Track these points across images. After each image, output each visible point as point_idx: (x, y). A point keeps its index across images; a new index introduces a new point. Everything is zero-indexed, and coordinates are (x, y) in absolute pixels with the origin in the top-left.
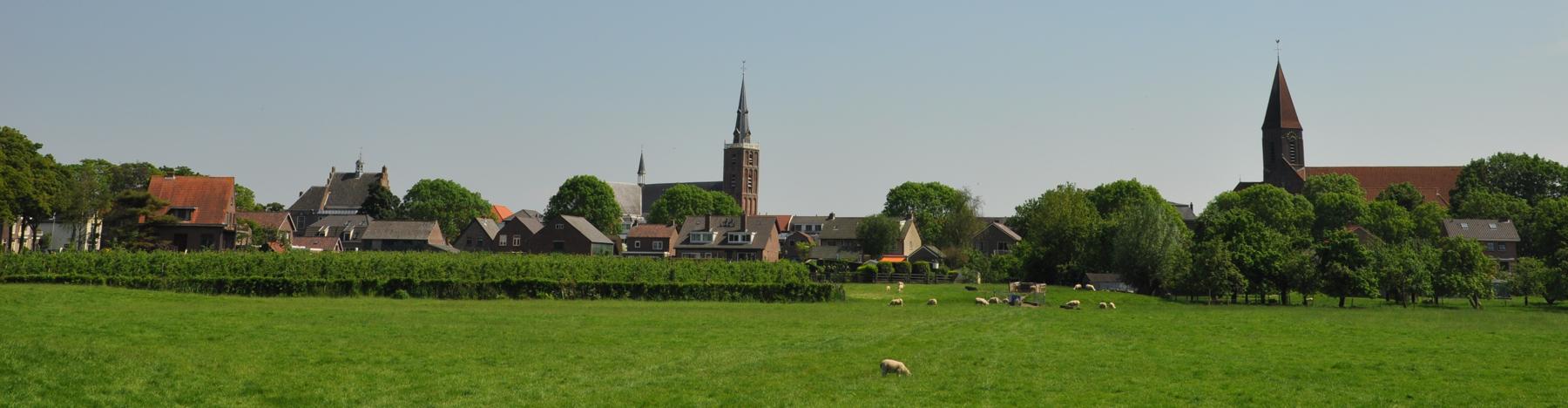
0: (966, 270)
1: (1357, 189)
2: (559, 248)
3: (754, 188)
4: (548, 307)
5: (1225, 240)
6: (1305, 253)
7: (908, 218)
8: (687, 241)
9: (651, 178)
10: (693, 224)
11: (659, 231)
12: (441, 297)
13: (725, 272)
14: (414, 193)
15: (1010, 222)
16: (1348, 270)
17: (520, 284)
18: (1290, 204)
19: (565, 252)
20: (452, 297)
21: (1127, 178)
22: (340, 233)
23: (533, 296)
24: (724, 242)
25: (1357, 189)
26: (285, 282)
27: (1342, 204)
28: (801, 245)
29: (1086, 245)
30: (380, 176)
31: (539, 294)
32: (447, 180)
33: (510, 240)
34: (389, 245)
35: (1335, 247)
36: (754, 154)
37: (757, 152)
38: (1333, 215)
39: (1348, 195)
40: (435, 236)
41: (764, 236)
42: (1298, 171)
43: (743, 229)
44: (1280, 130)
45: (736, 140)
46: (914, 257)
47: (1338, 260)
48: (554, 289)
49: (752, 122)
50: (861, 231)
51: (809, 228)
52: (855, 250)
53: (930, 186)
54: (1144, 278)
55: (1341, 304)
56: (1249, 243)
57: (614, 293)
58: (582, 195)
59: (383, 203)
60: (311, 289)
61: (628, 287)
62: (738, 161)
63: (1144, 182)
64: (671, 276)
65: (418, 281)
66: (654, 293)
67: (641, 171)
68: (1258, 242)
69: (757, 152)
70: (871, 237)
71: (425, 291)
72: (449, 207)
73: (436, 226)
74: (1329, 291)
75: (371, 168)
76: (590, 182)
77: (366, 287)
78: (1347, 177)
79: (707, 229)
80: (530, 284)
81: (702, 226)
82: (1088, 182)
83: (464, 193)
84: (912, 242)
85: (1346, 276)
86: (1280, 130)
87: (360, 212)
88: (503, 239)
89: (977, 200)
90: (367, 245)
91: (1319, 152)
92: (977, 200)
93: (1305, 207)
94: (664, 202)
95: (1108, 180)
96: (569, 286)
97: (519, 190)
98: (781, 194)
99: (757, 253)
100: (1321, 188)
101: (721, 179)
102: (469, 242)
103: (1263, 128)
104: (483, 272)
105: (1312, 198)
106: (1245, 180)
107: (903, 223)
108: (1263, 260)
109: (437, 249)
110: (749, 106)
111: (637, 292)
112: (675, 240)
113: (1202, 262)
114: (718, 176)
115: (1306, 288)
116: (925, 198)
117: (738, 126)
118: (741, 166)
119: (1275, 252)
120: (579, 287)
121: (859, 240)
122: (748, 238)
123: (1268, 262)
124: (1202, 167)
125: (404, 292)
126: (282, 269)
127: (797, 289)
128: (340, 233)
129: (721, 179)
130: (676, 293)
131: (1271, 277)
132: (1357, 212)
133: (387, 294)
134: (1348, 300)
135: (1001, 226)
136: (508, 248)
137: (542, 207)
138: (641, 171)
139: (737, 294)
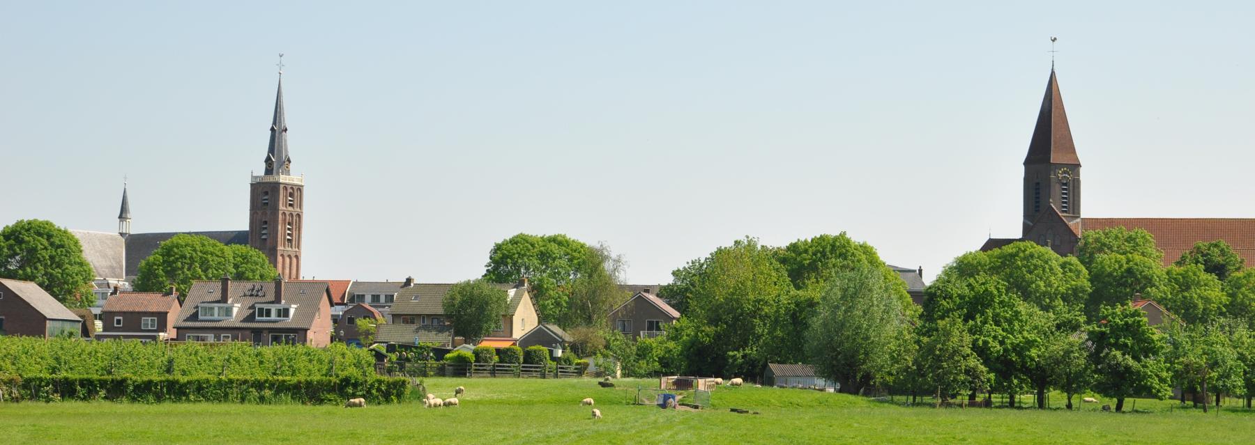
0: (601, 360)
1: (1151, 250)
3: (294, 240)
6: (1074, 338)
8: (194, 317)
9: (139, 225)
10: (202, 292)
11: (151, 302)
13: (246, 360)
15: (666, 293)
16: (1130, 361)
24: (251, 318)
27: (1129, 271)
28: (362, 323)
29: (743, 323)
37: (300, 189)
41: (310, 311)
42: (1071, 224)
43: (278, 300)
44: (1049, 166)
45: (269, 171)
47: (1117, 346)
49: (293, 144)
50: (449, 304)
51: (376, 298)
52: (441, 330)
53: (553, 240)
54: (850, 373)
55: (1119, 408)
56: (997, 323)
57: (81, 391)
61: (103, 384)
62: (269, 199)
63: (856, 237)
66: (143, 391)
69: (300, 189)
70: (467, 313)
74: (1102, 389)
79: (224, 299)
84: (525, 319)
85: (1128, 368)
86: (1049, 166)
89: (618, 261)
91: (1101, 198)
92: (618, 261)
98: (328, 252)
99: (298, 334)
101: (247, 228)
105: (1088, 263)
107: (512, 292)
108: (1015, 348)
110: (288, 120)
111: (117, 390)
112: (176, 315)
113: (931, 349)
115: (1072, 385)
116: (544, 257)
118: (276, 209)
119: (1031, 337)
121: (448, 317)
122: (286, 312)
123: (1020, 350)
124: (936, 215)
127: (355, 385)
129: (247, 228)
131: (1025, 369)
132: (1149, 281)
139: (267, 393)
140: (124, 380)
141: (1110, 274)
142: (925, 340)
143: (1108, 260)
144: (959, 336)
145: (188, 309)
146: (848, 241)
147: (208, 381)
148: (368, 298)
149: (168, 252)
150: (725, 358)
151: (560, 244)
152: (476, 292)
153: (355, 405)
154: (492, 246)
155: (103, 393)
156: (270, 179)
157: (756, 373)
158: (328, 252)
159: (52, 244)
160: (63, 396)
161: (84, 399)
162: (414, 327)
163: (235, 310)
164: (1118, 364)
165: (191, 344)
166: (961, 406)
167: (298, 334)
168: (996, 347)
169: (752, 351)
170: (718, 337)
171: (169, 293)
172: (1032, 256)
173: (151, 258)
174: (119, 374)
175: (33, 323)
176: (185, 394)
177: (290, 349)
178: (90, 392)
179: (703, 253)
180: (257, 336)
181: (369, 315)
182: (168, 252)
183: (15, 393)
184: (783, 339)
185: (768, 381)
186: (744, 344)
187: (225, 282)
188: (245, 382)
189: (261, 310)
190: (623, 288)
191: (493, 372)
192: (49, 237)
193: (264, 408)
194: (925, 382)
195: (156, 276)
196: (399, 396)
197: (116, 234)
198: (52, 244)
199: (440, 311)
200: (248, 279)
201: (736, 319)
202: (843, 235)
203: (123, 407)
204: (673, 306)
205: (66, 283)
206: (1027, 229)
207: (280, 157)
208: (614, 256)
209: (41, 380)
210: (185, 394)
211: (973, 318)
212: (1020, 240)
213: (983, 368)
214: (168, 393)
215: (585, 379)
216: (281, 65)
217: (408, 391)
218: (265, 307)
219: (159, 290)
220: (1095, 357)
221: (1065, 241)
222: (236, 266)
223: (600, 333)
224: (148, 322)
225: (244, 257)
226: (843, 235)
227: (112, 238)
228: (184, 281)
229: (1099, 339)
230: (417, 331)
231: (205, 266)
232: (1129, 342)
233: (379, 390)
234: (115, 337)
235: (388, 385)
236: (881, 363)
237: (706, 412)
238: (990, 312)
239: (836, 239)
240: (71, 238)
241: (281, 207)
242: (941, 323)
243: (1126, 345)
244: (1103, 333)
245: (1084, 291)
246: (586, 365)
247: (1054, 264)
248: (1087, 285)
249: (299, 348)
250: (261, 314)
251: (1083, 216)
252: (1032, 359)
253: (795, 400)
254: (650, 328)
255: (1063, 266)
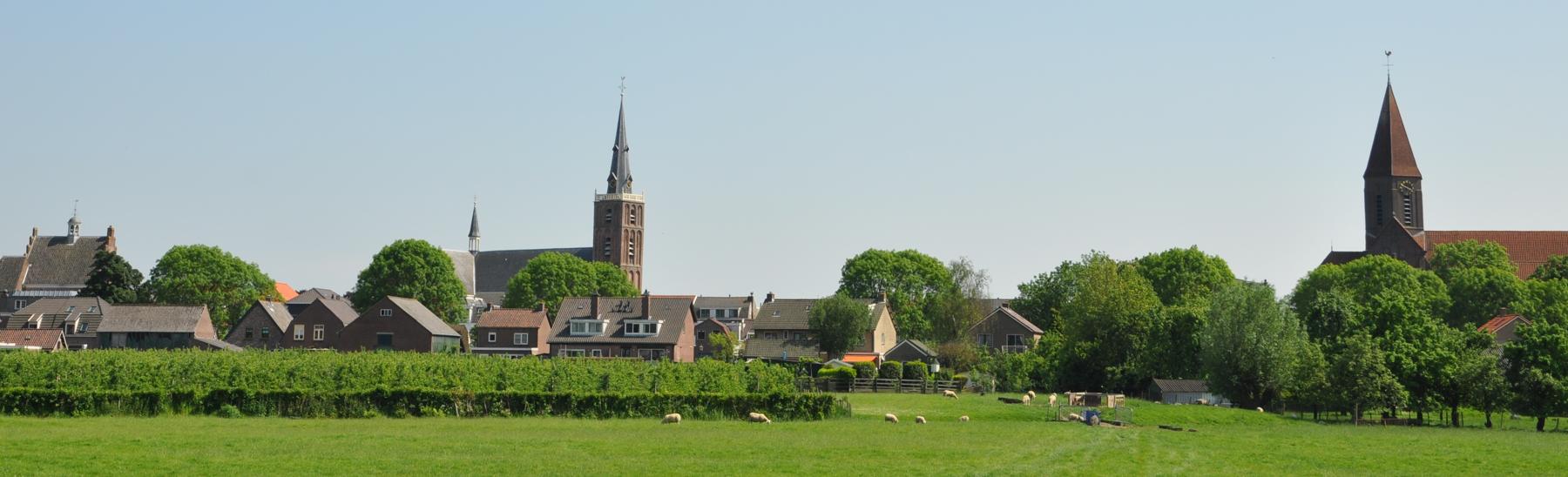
0: (977, 375)
1: (1506, 263)
2: (385, 343)
3: (636, 257)
4: (433, 428)
5: (1375, 334)
6: (1486, 355)
7: (877, 298)
8: (566, 332)
9: (487, 244)
10: (572, 308)
11: (521, 318)
12: (285, 414)
13: (627, 376)
14: (167, 265)
15: (1017, 305)
16: (1551, 380)
17: (397, 396)
18: (1413, 289)
19: (398, 348)
20: (300, 414)
21: (1184, 246)
22: (57, 322)
23: (417, 413)
24: (619, 333)
25: (1506, 263)
26: (62, 395)
27: (1491, 285)
28: (715, 338)
29: (1127, 338)
30: (104, 241)
31: (424, 409)
32: (210, 245)
33: (309, 331)
34: (138, 340)
35: (1534, 346)
36: (637, 209)
37: (641, 206)
38: (1472, 304)
39: (1498, 272)
40: (203, 326)
41: (675, 326)
42: (1415, 237)
43: (645, 316)
44: (1389, 177)
45: (612, 189)
46: (891, 355)
47: (1536, 363)
48: (443, 402)
49: (635, 164)
50: (815, 319)
51: (720, 313)
52: (807, 344)
53: (905, 255)
54: (1246, 387)
55: (1540, 427)
56: (1409, 340)
57: (529, 407)
58: (399, 270)
59: (118, 280)
60: (99, 406)
61: (549, 399)
62: (614, 220)
63: (1209, 250)
64: (604, 382)
65: (251, 393)
66: (584, 407)
67: (473, 233)
68: (1421, 338)
69: (641, 206)
70: (830, 328)
71: (262, 407)
72: (216, 283)
73: (204, 313)
74: (1520, 408)
75: (91, 229)
76: (419, 250)
77: (179, 401)
78: (1489, 245)
79: (594, 315)
80: (412, 396)
81: (588, 312)
82: (1128, 248)
83: (237, 266)
84: (885, 339)
85: (1549, 386)
86: (1389, 177)
87: (83, 294)
88: (299, 330)
89: (981, 276)
90: (105, 340)
91: (1445, 210)
92: (981, 276)
93: (1437, 287)
94: (520, 277)
95: (1157, 247)
96: (465, 397)
97: (317, 262)
98: (666, 268)
99: (662, 350)
100: (1455, 261)
101: (591, 245)
102: (249, 335)
103: (1367, 176)
104: (338, 378)
105: (1444, 275)
106: (1336, 249)
107: (872, 307)
108: (1429, 363)
109: (203, 346)
110: (630, 140)
111: (562, 405)
112: (545, 333)
113: (1344, 365)
114: (587, 242)
115: (1489, 403)
116: (898, 271)
117: (614, 169)
118: (619, 226)
119: (1445, 353)
120: (480, 399)
121: (810, 331)
122: (653, 328)
123: (1434, 367)
124: (1285, 233)
125: (233, 409)
126: (50, 377)
127: (785, 401)
128: (57, 322)
129: (591, 245)
130: (614, 407)
131: (1438, 386)
132: (1511, 295)
133: (208, 412)
134: (1549, 422)
135: (1010, 311)
136: (308, 342)
137: (347, 282)
138: (473, 233)
139: (701, 409)
140: (568, 396)
141: (1470, 288)
142: (1337, 357)
143: (1469, 275)
144: (1371, 352)
145: (560, 325)
146: (1201, 255)
147: (645, 397)
148: (713, 314)
149: (535, 270)
150: (1103, 374)
151: (912, 259)
152: (841, 307)
153: (753, 420)
154: (844, 263)
155: (549, 409)
156: (613, 197)
157: (1138, 388)
158: (666, 268)
159: (428, 263)
160: (513, 411)
161: (532, 414)
162: (781, 341)
163: (605, 326)
164: (1539, 383)
165: (563, 360)
166: (1372, 423)
167: (662, 350)
168: (1408, 363)
169: (1131, 366)
170: (1094, 353)
171: (539, 309)
172: (1389, 269)
173: (520, 275)
174: (563, 390)
175: (419, 339)
176: (623, 409)
177: (655, 366)
178: (537, 407)
179: (1049, 267)
180: (626, 350)
181: (719, 330)
182: (535, 270)
183: (470, 408)
184: (1161, 355)
185: (1156, 396)
186: (1122, 360)
187: (594, 298)
188: (680, 398)
189: (629, 325)
190: (988, 302)
191: (875, 387)
192: (426, 255)
193: (698, 422)
194: (1337, 398)
195: (525, 292)
196: (826, 411)
197: (466, 251)
198: (428, 263)
199: (807, 327)
200: (610, 295)
201: (1112, 333)
202: (1194, 248)
203: (568, 423)
204: (1026, 317)
205: (440, 299)
206: (1370, 242)
207: (622, 176)
208: (976, 270)
209: (492, 395)
210: (623, 409)
211: (1383, 335)
212: (583, 253)
213: (1398, 385)
214: (610, 407)
215: (988, 396)
216: (622, 88)
217: (833, 409)
218: (634, 322)
219: (527, 306)
220: (1512, 375)
221: (1414, 254)
222: (599, 283)
223: (967, 347)
224: (521, 338)
225: (606, 274)
226: (1194, 248)
227: (463, 256)
228: (553, 297)
229: (1515, 356)
230: (785, 344)
231: (570, 283)
232: (1548, 359)
233: (807, 406)
234: (490, 353)
235: (815, 401)
236: (1284, 376)
237: (1125, 430)
238: (1399, 328)
239: (1188, 252)
240: (444, 256)
241: (624, 224)
242: (1349, 341)
243: (1545, 363)
244: (1520, 351)
245: (1444, 305)
246: (965, 380)
247: (1413, 278)
248: (1447, 298)
249: (662, 365)
250: (629, 330)
251: (1427, 227)
252: (1447, 376)
253: (1212, 417)
254: (1011, 342)
255: (1421, 279)
